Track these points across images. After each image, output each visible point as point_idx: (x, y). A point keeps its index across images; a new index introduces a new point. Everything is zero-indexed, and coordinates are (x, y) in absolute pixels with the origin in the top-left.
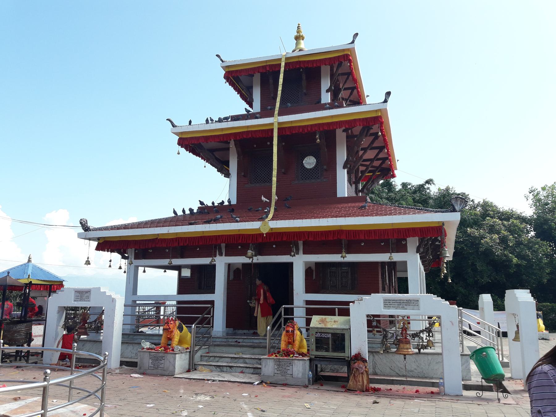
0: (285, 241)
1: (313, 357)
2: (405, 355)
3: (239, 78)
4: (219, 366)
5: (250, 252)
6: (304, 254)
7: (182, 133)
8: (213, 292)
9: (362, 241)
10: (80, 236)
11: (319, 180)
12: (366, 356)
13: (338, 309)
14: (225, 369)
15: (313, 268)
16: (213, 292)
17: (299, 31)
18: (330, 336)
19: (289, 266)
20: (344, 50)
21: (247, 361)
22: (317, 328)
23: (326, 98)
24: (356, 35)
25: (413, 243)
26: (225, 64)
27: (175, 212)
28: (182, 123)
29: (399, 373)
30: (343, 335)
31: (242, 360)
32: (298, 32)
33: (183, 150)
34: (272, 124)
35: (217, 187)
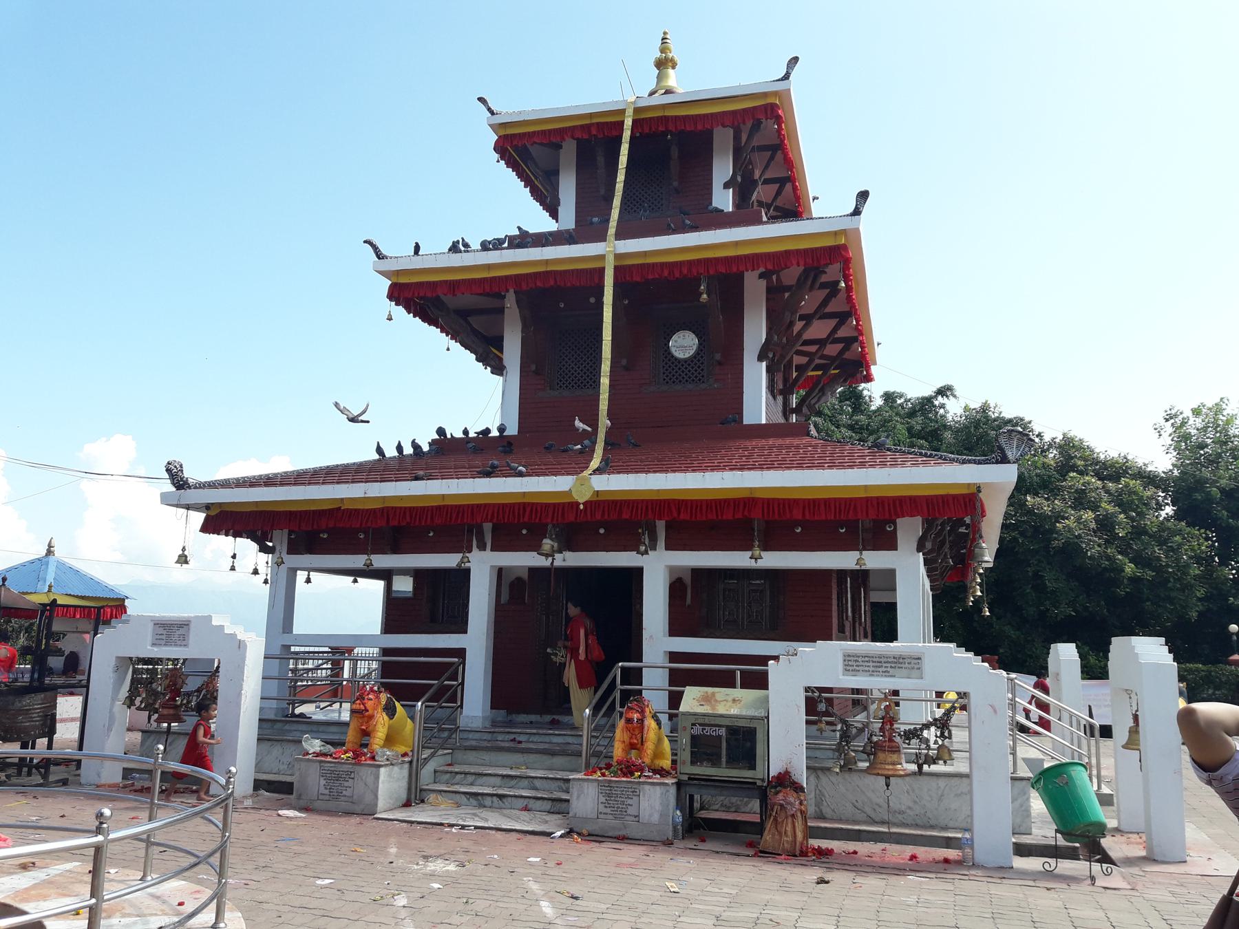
0: (626, 521)
1: (685, 778)
2: (887, 777)
3: (529, 150)
5: (547, 544)
6: (667, 549)
7: (398, 273)
10: (166, 499)
12: (802, 776)
13: (742, 672)
14: (488, 801)
15: (688, 580)
17: (664, 48)
18: (723, 732)
20: (765, 95)
21: (538, 783)
22: (695, 714)
23: (724, 200)
25: (909, 529)
26: (498, 120)
27: (379, 450)
28: (398, 250)
31: (526, 782)
33: (399, 311)
34: (602, 257)
35: (471, 395)
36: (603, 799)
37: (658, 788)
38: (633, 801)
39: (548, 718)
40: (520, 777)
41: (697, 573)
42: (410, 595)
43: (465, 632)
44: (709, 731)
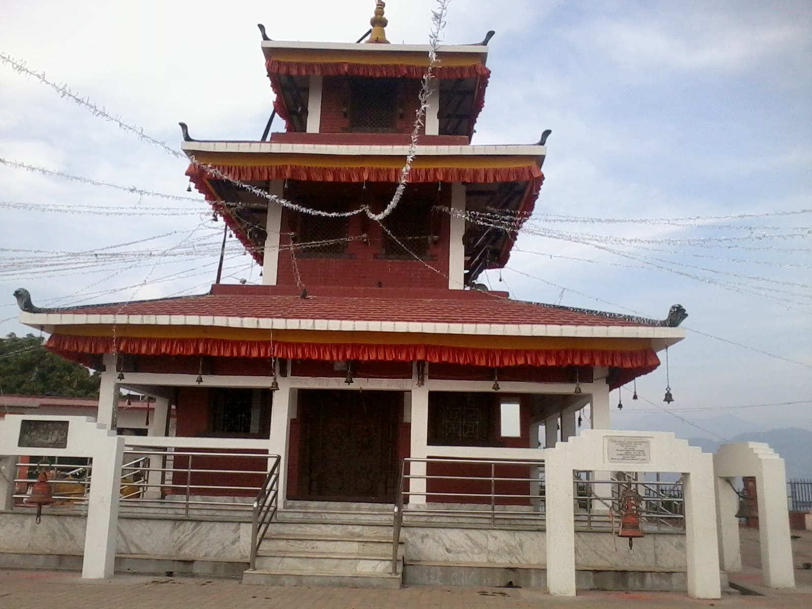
8: (264, 434)
16: (264, 434)
43: (428, 444)
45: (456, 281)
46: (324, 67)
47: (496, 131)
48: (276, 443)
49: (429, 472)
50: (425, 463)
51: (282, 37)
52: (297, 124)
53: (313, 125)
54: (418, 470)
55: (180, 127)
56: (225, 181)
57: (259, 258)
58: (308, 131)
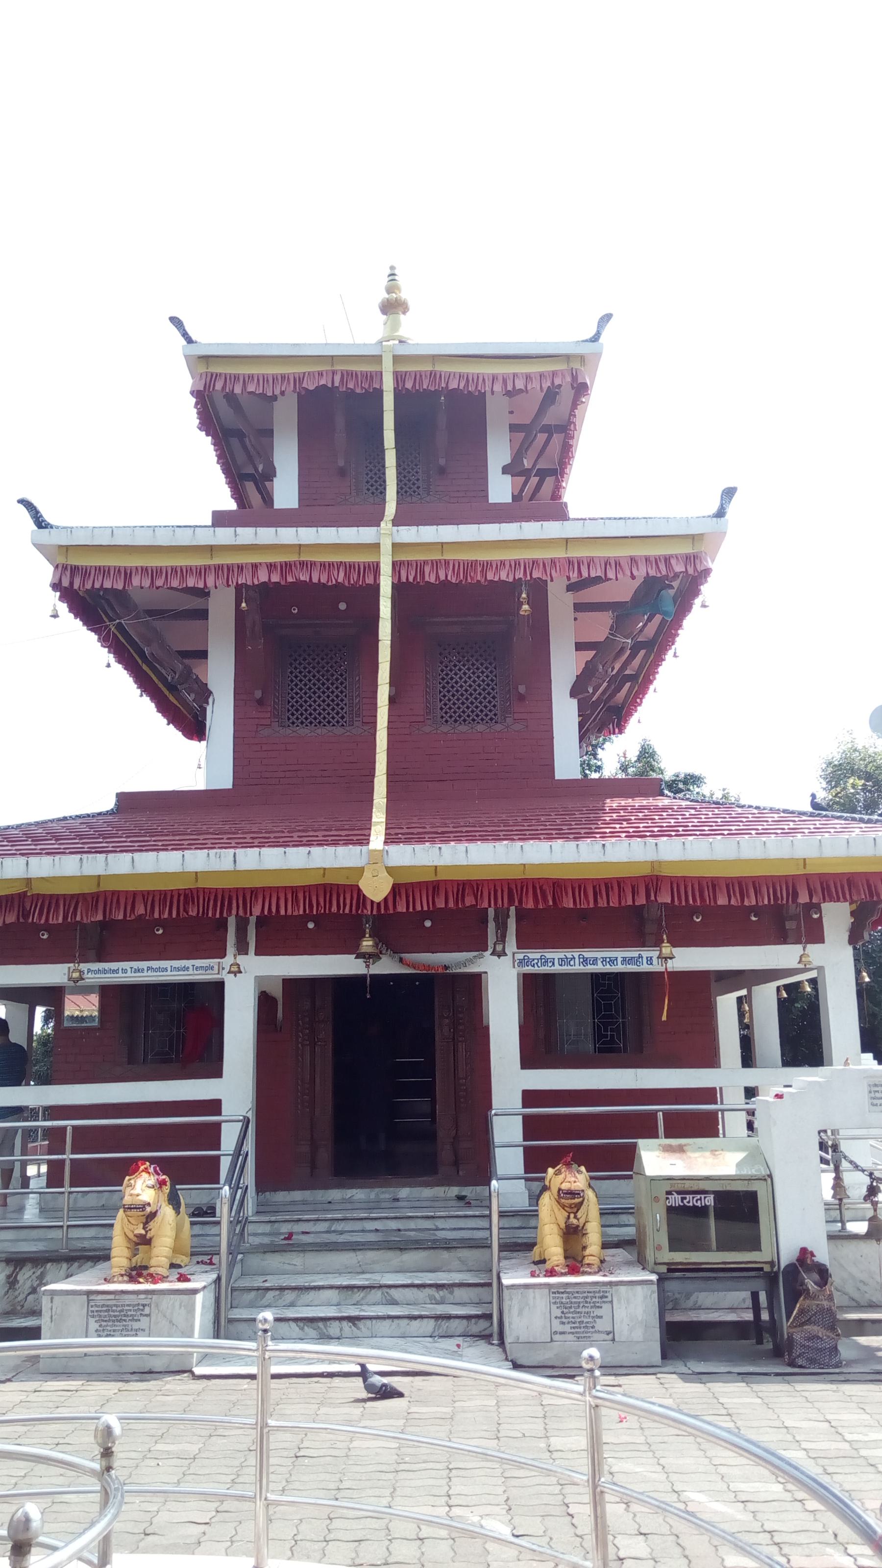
0: (460, 911)
1: (663, 1269)
4: (311, 1320)
5: (367, 944)
6: (256, 954)
7: (66, 549)
8: (216, 1072)
9: (694, 911)
11: (499, 727)
12: (822, 1254)
13: (666, 1114)
14: (334, 1328)
15: (277, 992)
16: (216, 1072)
17: (392, 286)
18: (710, 1200)
19: (474, 985)
20: (567, 358)
21: (396, 1294)
22: (670, 1179)
23: (500, 489)
24: (607, 317)
25: (836, 917)
29: (856, 1295)
30: (752, 1197)
31: (377, 1295)
32: (389, 290)
34: (375, 547)
36: (558, 1313)
37: (639, 1288)
38: (605, 1310)
39: (455, 1191)
40: (371, 1287)
41: (291, 984)
42: (96, 1023)
43: (522, 1068)
44: (691, 1201)
45: (567, 763)
46: (299, 379)
47: (615, 485)
48: (234, 1087)
49: (528, 1134)
50: (522, 1148)
51: (219, 333)
52: (255, 497)
53: (286, 492)
54: (507, 1131)
55: (21, 507)
56: (127, 607)
57: (193, 726)
58: (276, 507)
